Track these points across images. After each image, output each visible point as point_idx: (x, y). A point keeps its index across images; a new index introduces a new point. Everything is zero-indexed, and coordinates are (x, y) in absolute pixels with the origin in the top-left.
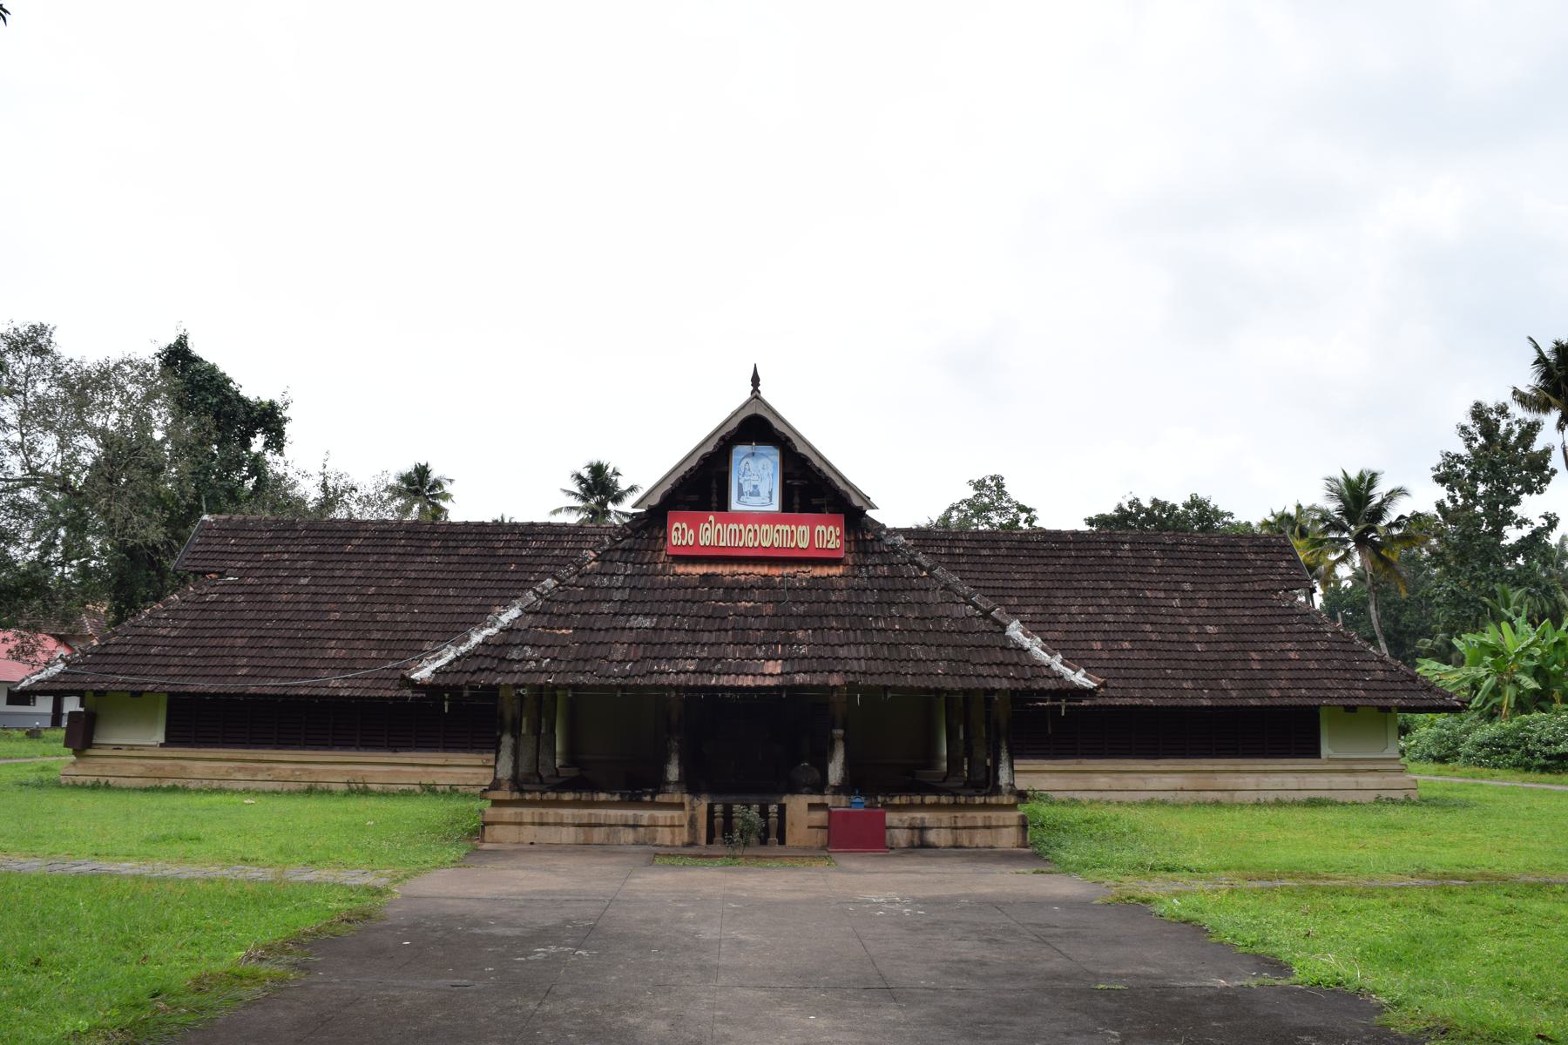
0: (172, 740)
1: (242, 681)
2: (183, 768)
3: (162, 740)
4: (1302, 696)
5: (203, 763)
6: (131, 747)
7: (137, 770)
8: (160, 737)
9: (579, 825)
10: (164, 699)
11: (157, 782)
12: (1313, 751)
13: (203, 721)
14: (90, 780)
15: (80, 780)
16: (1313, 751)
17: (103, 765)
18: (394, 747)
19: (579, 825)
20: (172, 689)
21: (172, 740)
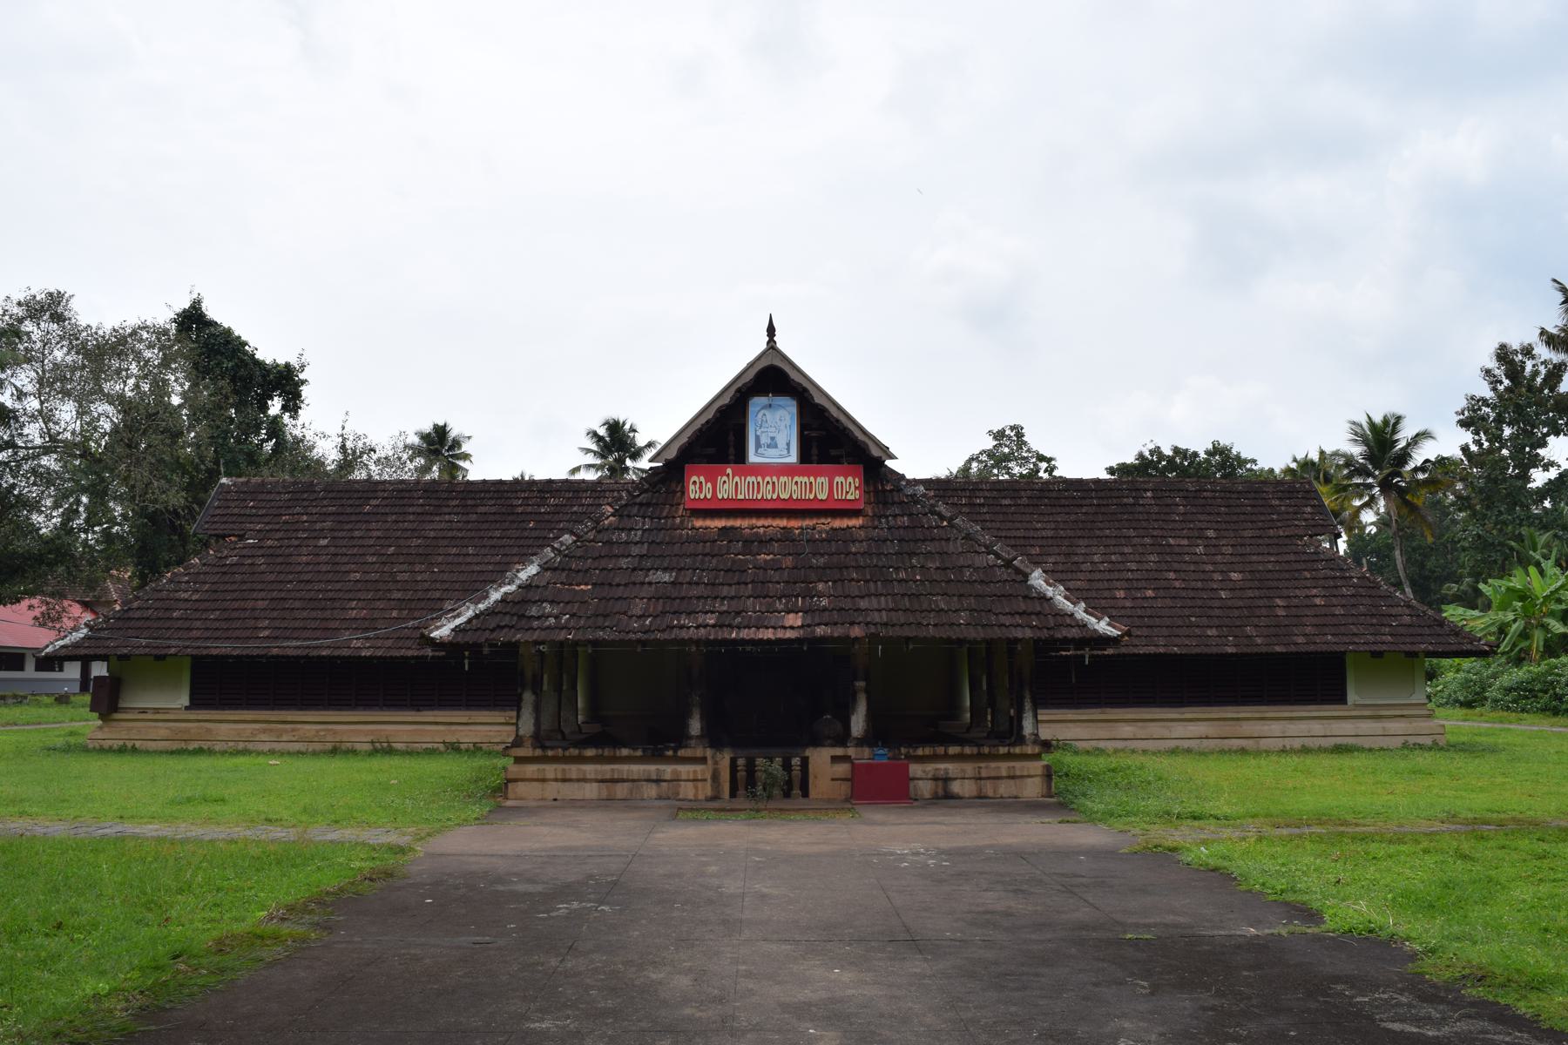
0: (196, 703)
1: (266, 641)
2: (209, 731)
3: (187, 703)
4: (1328, 642)
5: (228, 725)
6: (157, 711)
7: (163, 733)
8: (185, 700)
9: (602, 781)
10: (187, 663)
11: (183, 745)
12: (1341, 699)
13: (227, 683)
14: (116, 744)
15: (107, 744)
16: (1341, 699)
17: (130, 729)
18: (417, 705)
19: (602, 781)
20: (195, 652)
21: (196, 703)
